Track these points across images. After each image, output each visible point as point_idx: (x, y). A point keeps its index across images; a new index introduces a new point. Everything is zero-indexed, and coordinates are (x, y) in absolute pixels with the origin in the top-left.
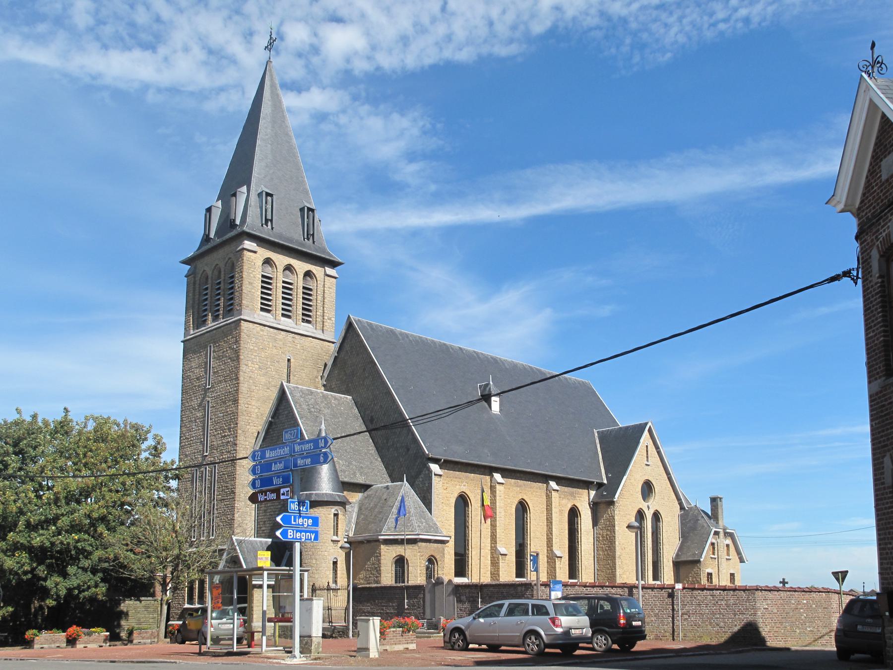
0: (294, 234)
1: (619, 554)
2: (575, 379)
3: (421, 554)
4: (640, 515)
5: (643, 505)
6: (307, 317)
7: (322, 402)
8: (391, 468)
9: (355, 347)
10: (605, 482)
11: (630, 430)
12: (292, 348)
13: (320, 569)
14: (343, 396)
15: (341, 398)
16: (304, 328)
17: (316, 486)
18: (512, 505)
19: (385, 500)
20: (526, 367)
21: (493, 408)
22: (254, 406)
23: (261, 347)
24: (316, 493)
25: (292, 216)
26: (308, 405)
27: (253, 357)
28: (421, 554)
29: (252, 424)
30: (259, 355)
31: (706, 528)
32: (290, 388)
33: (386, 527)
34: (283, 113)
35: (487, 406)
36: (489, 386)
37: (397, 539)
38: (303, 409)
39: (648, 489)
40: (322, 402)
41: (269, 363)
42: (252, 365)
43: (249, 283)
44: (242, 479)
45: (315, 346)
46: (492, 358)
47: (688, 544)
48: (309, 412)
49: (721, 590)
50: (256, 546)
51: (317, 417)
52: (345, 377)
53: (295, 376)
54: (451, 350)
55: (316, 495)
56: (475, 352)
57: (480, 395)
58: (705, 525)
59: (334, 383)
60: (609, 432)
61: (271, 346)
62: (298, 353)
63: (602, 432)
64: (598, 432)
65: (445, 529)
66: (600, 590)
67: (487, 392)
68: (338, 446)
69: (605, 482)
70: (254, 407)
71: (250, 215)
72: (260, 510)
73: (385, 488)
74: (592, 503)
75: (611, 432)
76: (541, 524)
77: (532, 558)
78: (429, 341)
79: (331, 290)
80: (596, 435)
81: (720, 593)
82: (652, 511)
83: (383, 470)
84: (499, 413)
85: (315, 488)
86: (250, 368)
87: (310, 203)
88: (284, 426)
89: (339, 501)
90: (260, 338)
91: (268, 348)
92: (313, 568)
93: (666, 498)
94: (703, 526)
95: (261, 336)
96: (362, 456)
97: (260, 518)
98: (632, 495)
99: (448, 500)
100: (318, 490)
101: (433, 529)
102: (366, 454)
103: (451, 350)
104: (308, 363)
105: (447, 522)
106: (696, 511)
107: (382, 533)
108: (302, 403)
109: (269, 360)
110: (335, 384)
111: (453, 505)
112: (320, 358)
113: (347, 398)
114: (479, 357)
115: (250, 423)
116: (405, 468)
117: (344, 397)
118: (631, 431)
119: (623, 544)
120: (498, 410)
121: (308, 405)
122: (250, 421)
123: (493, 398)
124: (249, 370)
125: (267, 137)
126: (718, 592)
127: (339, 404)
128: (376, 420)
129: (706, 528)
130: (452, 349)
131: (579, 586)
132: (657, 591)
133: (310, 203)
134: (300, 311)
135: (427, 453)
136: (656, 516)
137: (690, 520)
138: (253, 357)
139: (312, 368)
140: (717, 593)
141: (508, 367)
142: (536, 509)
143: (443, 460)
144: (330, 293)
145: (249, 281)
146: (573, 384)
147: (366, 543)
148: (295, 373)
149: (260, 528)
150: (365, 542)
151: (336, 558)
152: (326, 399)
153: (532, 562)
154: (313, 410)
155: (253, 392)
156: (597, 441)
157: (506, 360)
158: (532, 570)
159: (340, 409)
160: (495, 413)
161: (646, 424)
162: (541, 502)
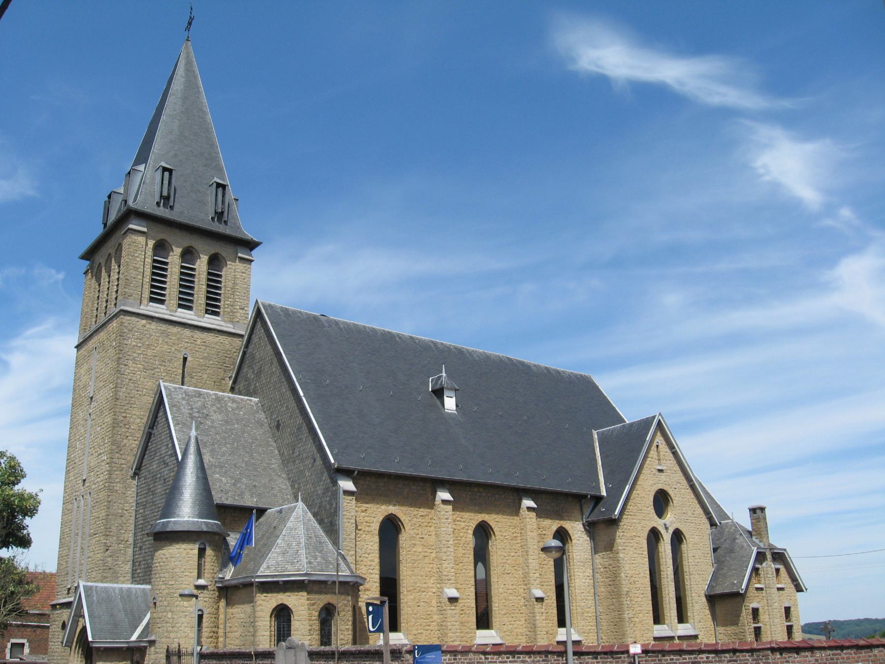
0: (204, 218)
1: (626, 589)
2: (572, 373)
3: (312, 602)
4: (654, 536)
5: (659, 523)
6: (212, 306)
7: (212, 405)
8: (296, 486)
9: (263, 337)
10: (604, 493)
11: (635, 427)
12: (189, 344)
13: (178, 625)
14: (246, 398)
15: (242, 400)
16: (209, 321)
17: (176, 511)
18: (467, 530)
19: (275, 527)
20: (503, 359)
21: (446, 406)
22: (135, 415)
23: (147, 343)
24: (174, 521)
25: (198, 194)
26: (192, 409)
27: (135, 355)
28: (312, 602)
29: (131, 438)
30: (144, 353)
31: (746, 549)
32: (170, 389)
33: (265, 565)
34: (199, 89)
35: (439, 403)
36: (442, 379)
37: (277, 582)
38: (182, 414)
39: (662, 501)
40: (212, 405)
41: (157, 363)
42: (134, 365)
43: (135, 267)
44: (114, 508)
45: (221, 341)
46: (456, 348)
47: (725, 571)
48: (190, 417)
49: (710, 652)
50: (113, 594)
51: (201, 423)
52: (253, 376)
53: (192, 378)
54: (397, 339)
55: (174, 523)
56: (432, 342)
57: (430, 390)
58: (745, 544)
59: (242, 385)
60: (610, 432)
61: (160, 342)
62: (198, 350)
63: (603, 433)
64: (597, 433)
65: (365, 565)
66: (508, 658)
67: (438, 387)
68: (224, 460)
69: (604, 493)
70: (134, 417)
71: (143, 193)
72: (136, 547)
73: (278, 512)
74: (586, 524)
75: (612, 431)
76: (512, 554)
77: (371, 609)
78: (367, 329)
79: (244, 275)
80: (596, 436)
81: (707, 658)
82: (671, 531)
83: (288, 488)
84: (456, 412)
85: (175, 513)
86: (130, 369)
87: (223, 180)
88: (161, 437)
89: (205, 530)
90: (146, 332)
91: (157, 344)
92: (168, 624)
93: (690, 513)
94: (742, 547)
95: (147, 331)
96: (258, 471)
97: (137, 557)
98: (641, 510)
99: (368, 526)
100: (178, 516)
101: (332, 566)
102: (264, 469)
103: (397, 339)
104: (211, 362)
105: (367, 555)
106: (733, 528)
107: (259, 574)
108: (182, 407)
109: (157, 358)
110: (244, 386)
111: (377, 532)
112: (229, 356)
113: (251, 400)
114: (437, 348)
115: (127, 437)
116: (311, 485)
117: (248, 399)
118: (636, 427)
119: (632, 577)
120: (454, 407)
121: (192, 409)
122: (127, 434)
123: (446, 393)
124: (129, 371)
125: (175, 113)
126: (704, 656)
127: (237, 407)
128: (282, 425)
129: (746, 549)
130: (400, 338)
131: (475, 652)
132: (601, 658)
133: (223, 179)
134: (203, 301)
135: (333, 461)
136: (678, 537)
137: (726, 540)
138: (135, 355)
139: (218, 368)
140: (701, 658)
141: (477, 359)
142: (504, 534)
143: (356, 472)
144: (244, 279)
145: (135, 265)
146: (568, 378)
147: (242, 588)
148: (194, 374)
149: (136, 570)
150: (241, 587)
151: (200, 610)
152: (219, 401)
153: (370, 617)
154: (197, 415)
155: (134, 397)
156: (597, 444)
157: (476, 351)
158: (371, 629)
159: (239, 414)
160: (450, 411)
161: (654, 417)
162: (511, 524)
